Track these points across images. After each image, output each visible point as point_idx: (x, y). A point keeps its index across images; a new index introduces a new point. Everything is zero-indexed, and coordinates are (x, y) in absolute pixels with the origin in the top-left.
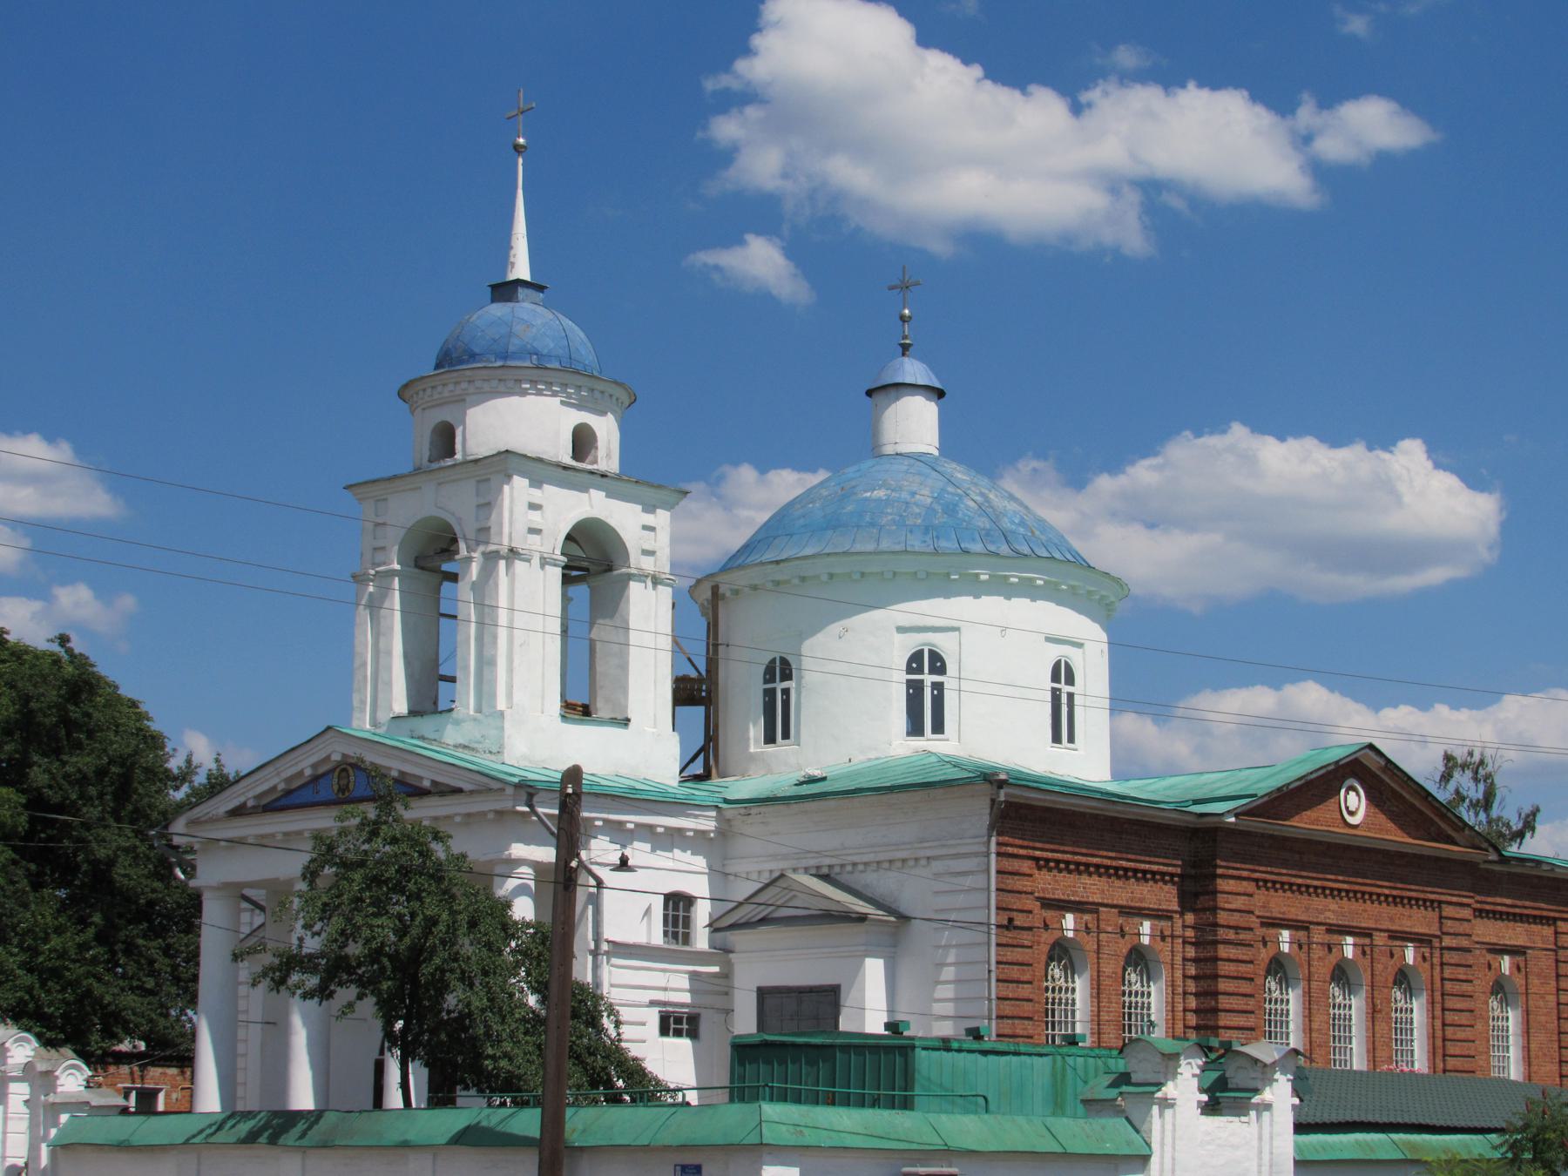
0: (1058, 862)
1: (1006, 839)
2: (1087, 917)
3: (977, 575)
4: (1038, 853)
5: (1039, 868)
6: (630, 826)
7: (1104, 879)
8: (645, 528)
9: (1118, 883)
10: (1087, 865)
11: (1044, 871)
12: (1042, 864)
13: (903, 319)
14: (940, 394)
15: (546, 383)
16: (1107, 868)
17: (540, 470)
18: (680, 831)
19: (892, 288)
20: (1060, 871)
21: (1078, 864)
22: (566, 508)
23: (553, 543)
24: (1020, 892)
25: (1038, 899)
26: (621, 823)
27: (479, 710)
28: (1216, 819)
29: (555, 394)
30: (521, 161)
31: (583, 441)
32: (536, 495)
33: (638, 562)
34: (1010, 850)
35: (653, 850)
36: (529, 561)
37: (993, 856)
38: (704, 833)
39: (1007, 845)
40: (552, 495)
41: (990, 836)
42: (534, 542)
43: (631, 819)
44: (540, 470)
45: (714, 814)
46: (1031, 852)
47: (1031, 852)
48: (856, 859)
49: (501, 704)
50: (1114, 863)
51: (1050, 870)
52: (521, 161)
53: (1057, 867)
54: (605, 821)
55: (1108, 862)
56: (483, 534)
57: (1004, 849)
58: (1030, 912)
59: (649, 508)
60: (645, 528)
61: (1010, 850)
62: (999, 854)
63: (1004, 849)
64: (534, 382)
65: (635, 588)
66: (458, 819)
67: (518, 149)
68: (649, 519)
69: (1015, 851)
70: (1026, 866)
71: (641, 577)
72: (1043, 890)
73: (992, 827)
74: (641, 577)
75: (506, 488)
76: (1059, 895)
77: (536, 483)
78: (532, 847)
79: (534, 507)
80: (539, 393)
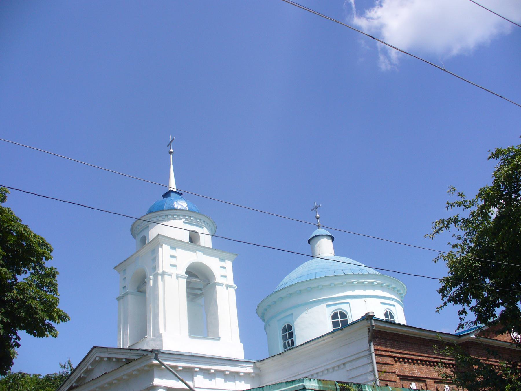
0: (404, 358)
1: (378, 347)
2: (421, 384)
3: (352, 283)
4: (394, 354)
5: (396, 362)
6: (213, 371)
7: (425, 366)
8: (221, 267)
9: (431, 368)
10: (417, 360)
11: (398, 363)
12: (397, 359)
13: (317, 218)
14: (333, 239)
15: (177, 215)
16: (426, 361)
17: (174, 244)
18: (238, 373)
19: (312, 210)
20: (405, 363)
21: (413, 359)
22: (187, 258)
23: (182, 271)
24: (389, 372)
25: (398, 376)
26: (209, 370)
27: (154, 335)
28: (467, 337)
29: (181, 219)
30: (171, 156)
31: (193, 238)
32: (173, 252)
33: (218, 279)
34: (381, 353)
35: (225, 381)
36: (171, 275)
37: (373, 355)
38: (249, 374)
39: (379, 350)
40: (179, 252)
41: (370, 345)
42: (173, 271)
43: (213, 368)
44: (174, 244)
45: (252, 365)
46: (391, 354)
47: (391, 354)
48: (312, 372)
49: (161, 331)
50: (428, 359)
51: (401, 362)
52: (171, 156)
53: (403, 361)
54: (200, 369)
55: (425, 359)
56: (155, 268)
57: (378, 352)
58: (395, 382)
59: (223, 260)
60: (221, 267)
61: (381, 353)
62: (376, 355)
63: (378, 352)
64: (172, 215)
65: (218, 288)
66: (114, 360)
67: (170, 153)
68: (223, 264)
69: (384, 353)
70: (390, 360)
71: (221, 285)
72: (399, 371)
73: (370, 342)
74: (221, 285)
75: (160, 249)
76: (406, 374)
77: (173, 248)
78: (164, 380)
79: (172, 256)
80: (175, 219)
